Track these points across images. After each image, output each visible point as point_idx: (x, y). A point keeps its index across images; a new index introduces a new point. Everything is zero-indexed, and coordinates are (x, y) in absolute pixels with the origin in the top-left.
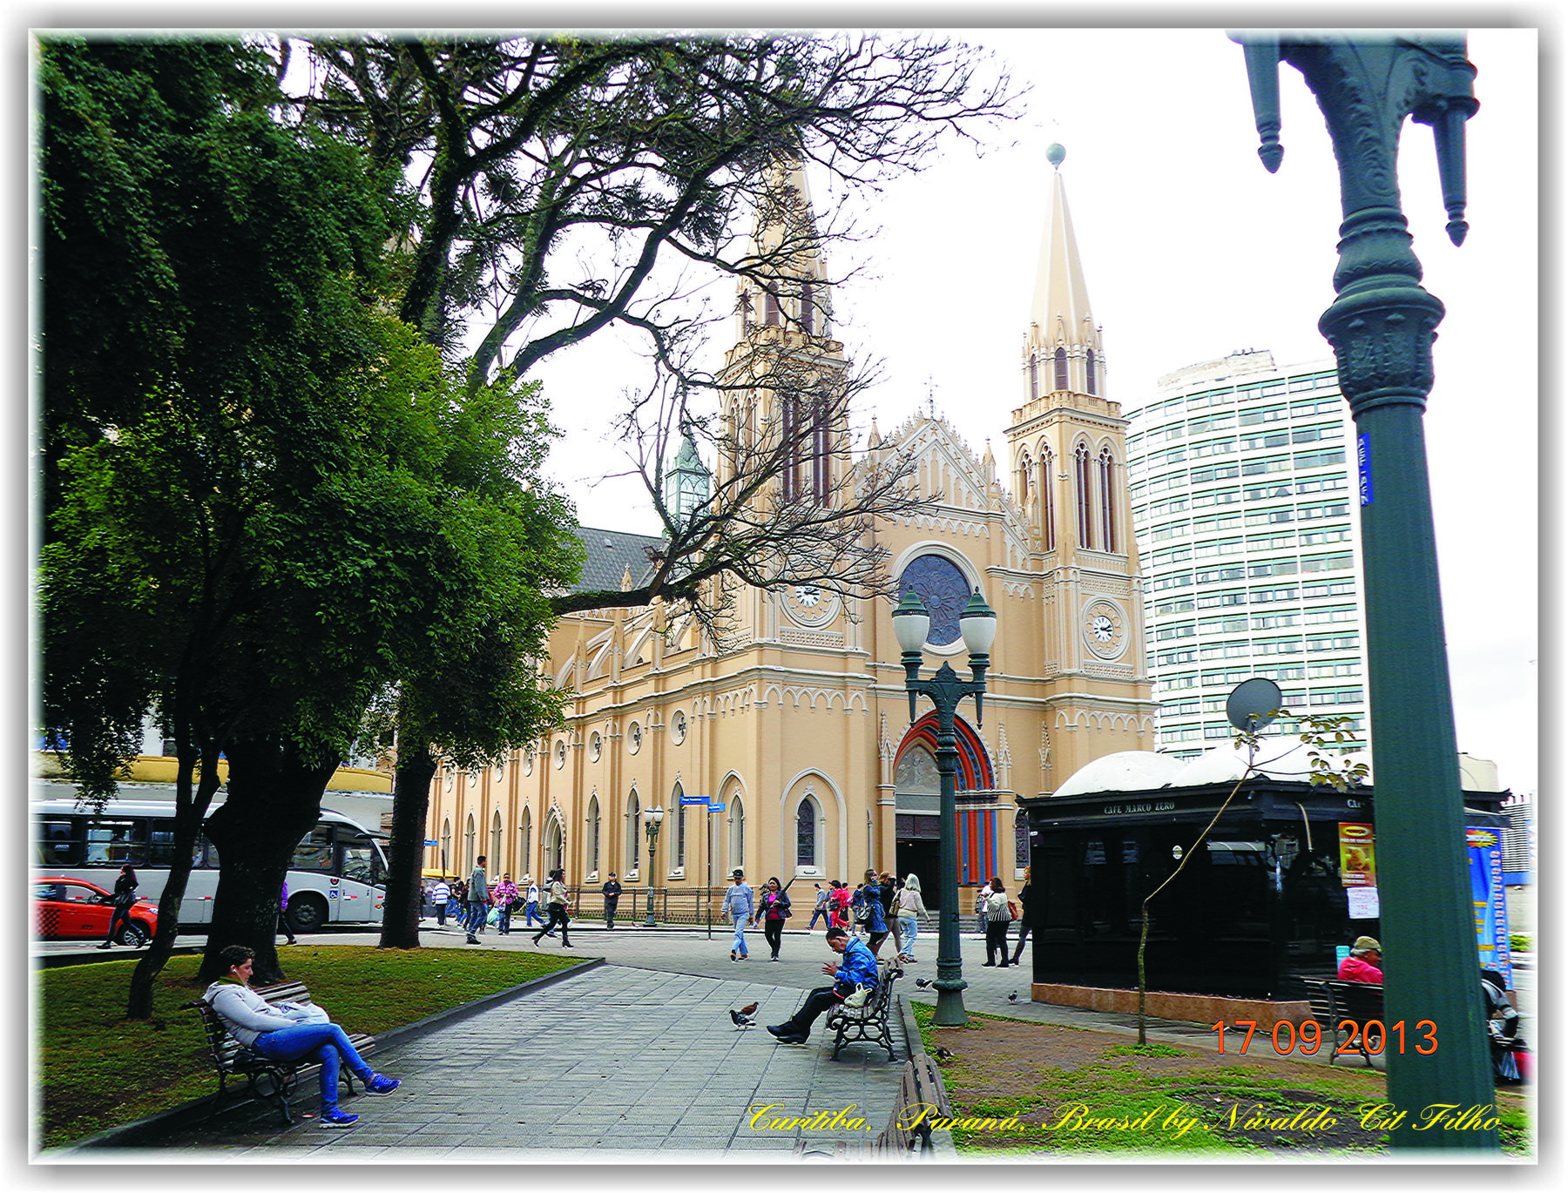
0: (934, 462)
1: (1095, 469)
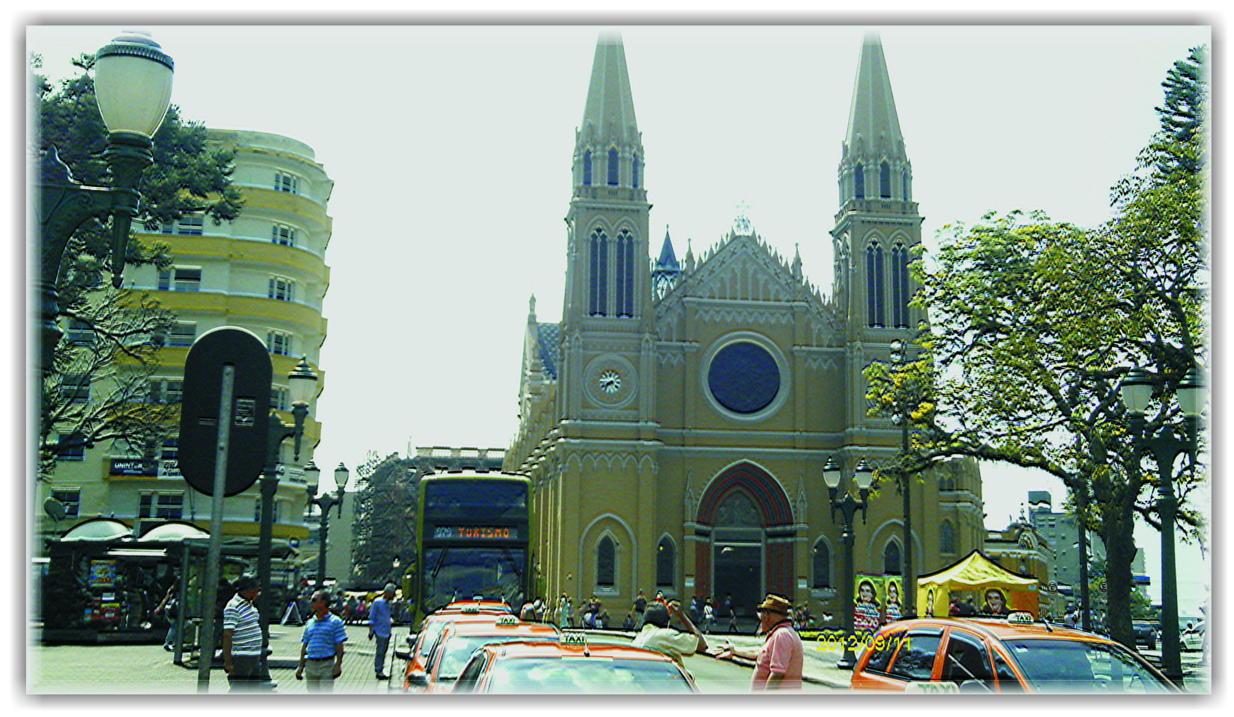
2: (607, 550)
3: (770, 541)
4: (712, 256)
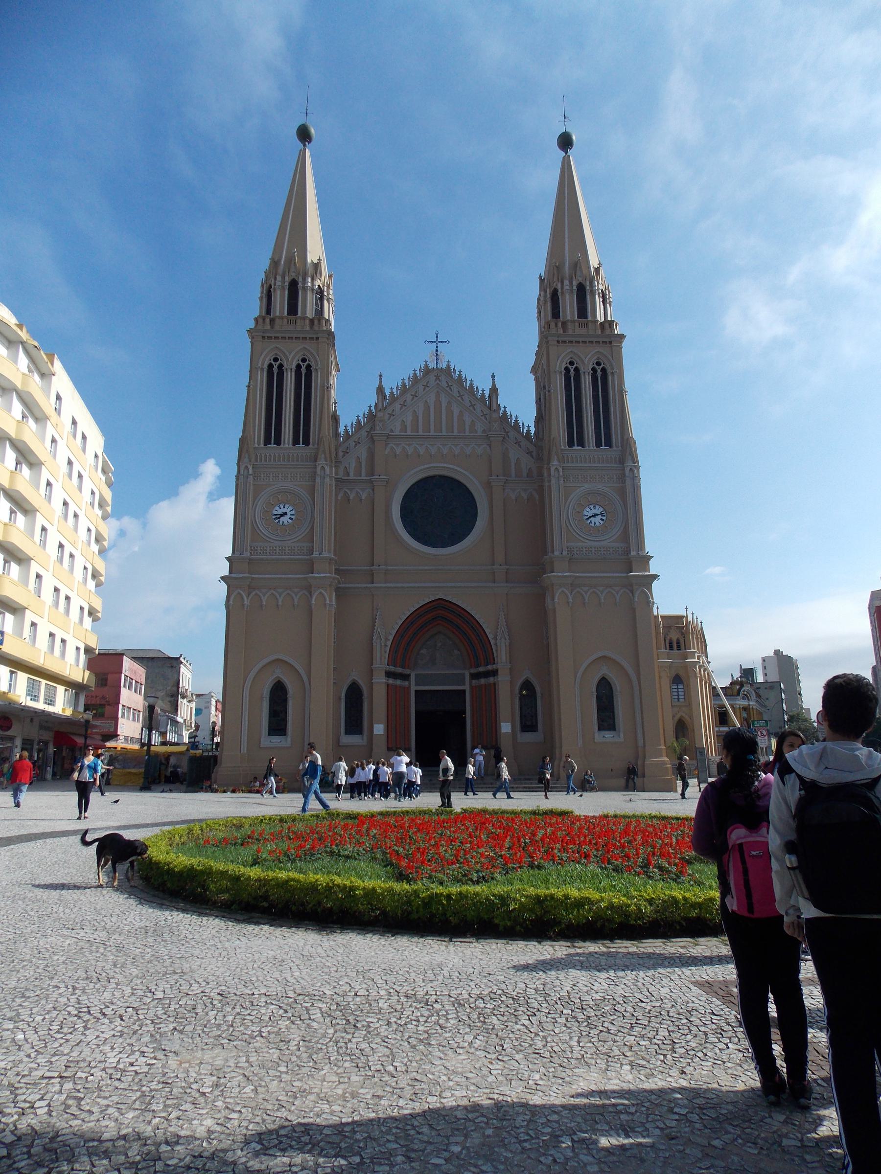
1: (587, 383)
2: (279, 694)
4: (404, 389)
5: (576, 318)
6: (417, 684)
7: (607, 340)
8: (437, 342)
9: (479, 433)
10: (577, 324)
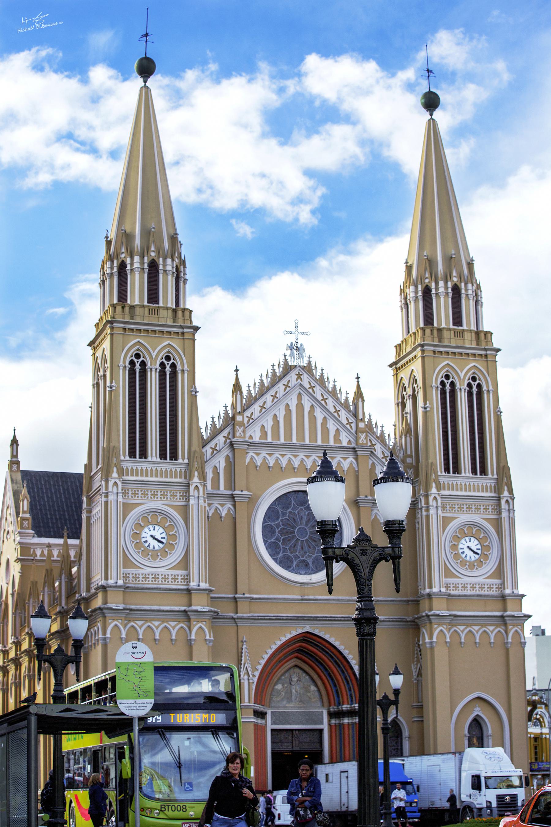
0: (300, 406)
3: (333, 722)
5: (146, 303)
6: (273, 723)
7: (483, 353)
8: (296, 331)
9: (345, 444)
10: (147, 310)
